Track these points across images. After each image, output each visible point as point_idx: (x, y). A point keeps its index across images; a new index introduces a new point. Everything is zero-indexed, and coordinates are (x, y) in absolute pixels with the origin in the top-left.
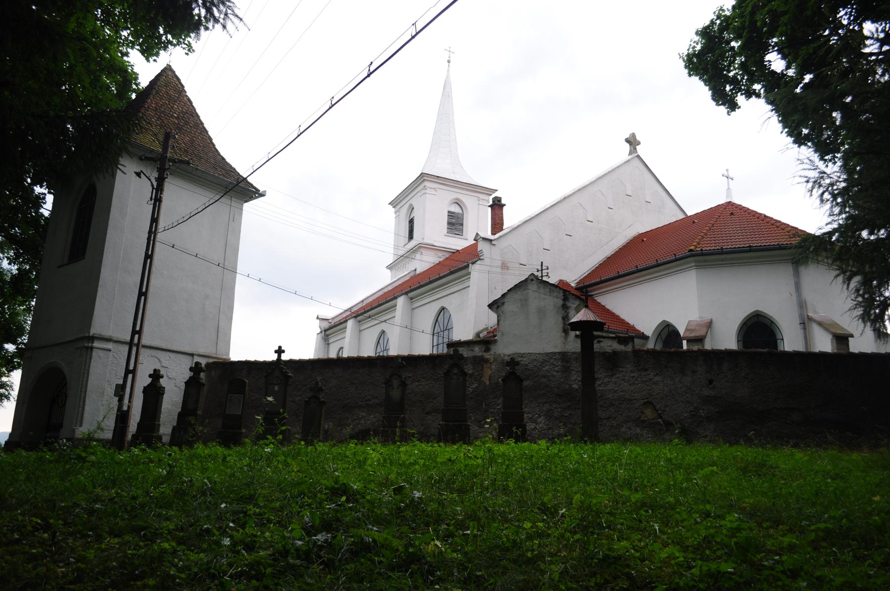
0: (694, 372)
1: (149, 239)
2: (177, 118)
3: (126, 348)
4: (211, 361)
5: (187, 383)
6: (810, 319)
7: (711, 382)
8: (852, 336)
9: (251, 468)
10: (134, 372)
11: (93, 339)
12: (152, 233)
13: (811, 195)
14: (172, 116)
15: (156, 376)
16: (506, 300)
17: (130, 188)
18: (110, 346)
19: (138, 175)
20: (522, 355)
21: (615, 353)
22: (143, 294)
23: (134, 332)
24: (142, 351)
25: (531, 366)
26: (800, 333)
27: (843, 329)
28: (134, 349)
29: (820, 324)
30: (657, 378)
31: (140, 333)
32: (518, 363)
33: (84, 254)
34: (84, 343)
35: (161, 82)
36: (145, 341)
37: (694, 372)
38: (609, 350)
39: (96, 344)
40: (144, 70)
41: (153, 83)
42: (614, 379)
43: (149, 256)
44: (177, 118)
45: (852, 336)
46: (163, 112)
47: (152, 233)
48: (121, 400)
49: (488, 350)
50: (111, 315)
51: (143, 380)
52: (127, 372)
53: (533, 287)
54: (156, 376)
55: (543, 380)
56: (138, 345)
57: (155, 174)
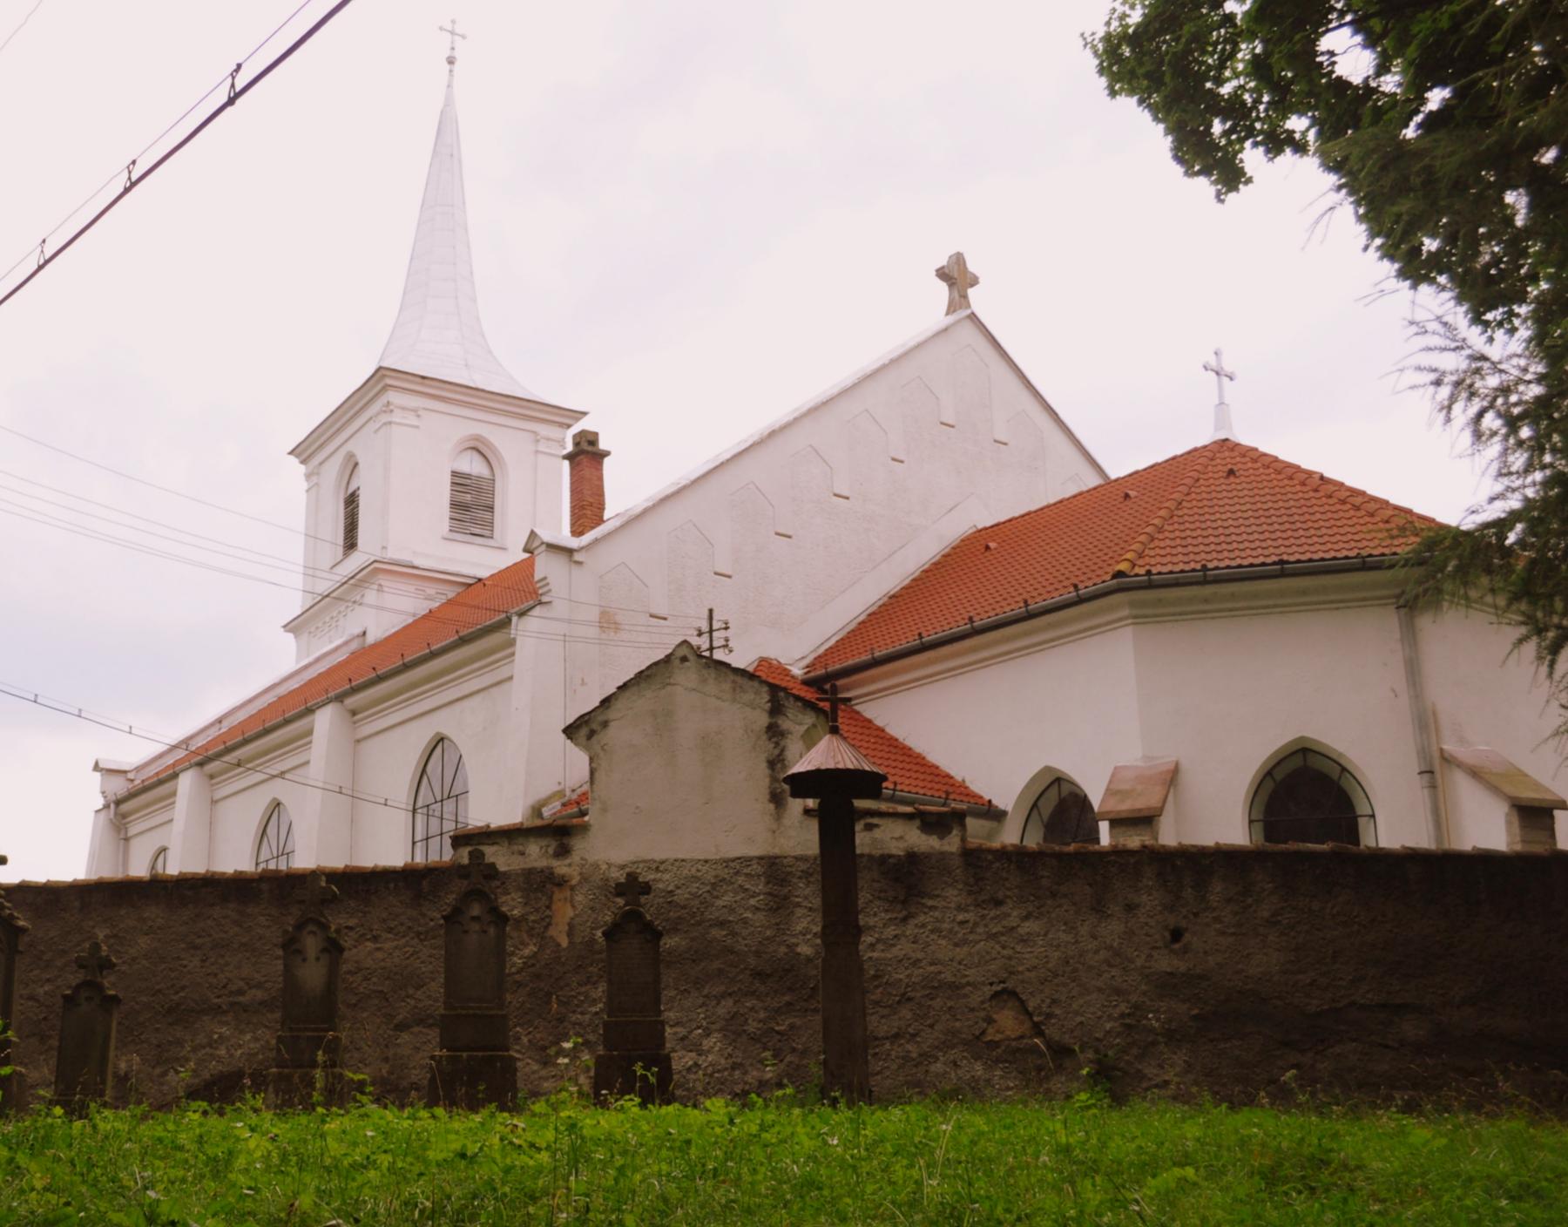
0: (1130, 908)
6: (1448, 760)
7: (1176, 935)
16: (612, 714)
20: (658, 866)
21: (912, 857)
25: (681, 896)
27: (1548, 790)
29: (1475, 773)
32: (646, 888)
37: (1130, 908)
38: (897, 849)
42: (910, 929)
49: (563, 852)
53: (686, 677)
55: (717, 933)
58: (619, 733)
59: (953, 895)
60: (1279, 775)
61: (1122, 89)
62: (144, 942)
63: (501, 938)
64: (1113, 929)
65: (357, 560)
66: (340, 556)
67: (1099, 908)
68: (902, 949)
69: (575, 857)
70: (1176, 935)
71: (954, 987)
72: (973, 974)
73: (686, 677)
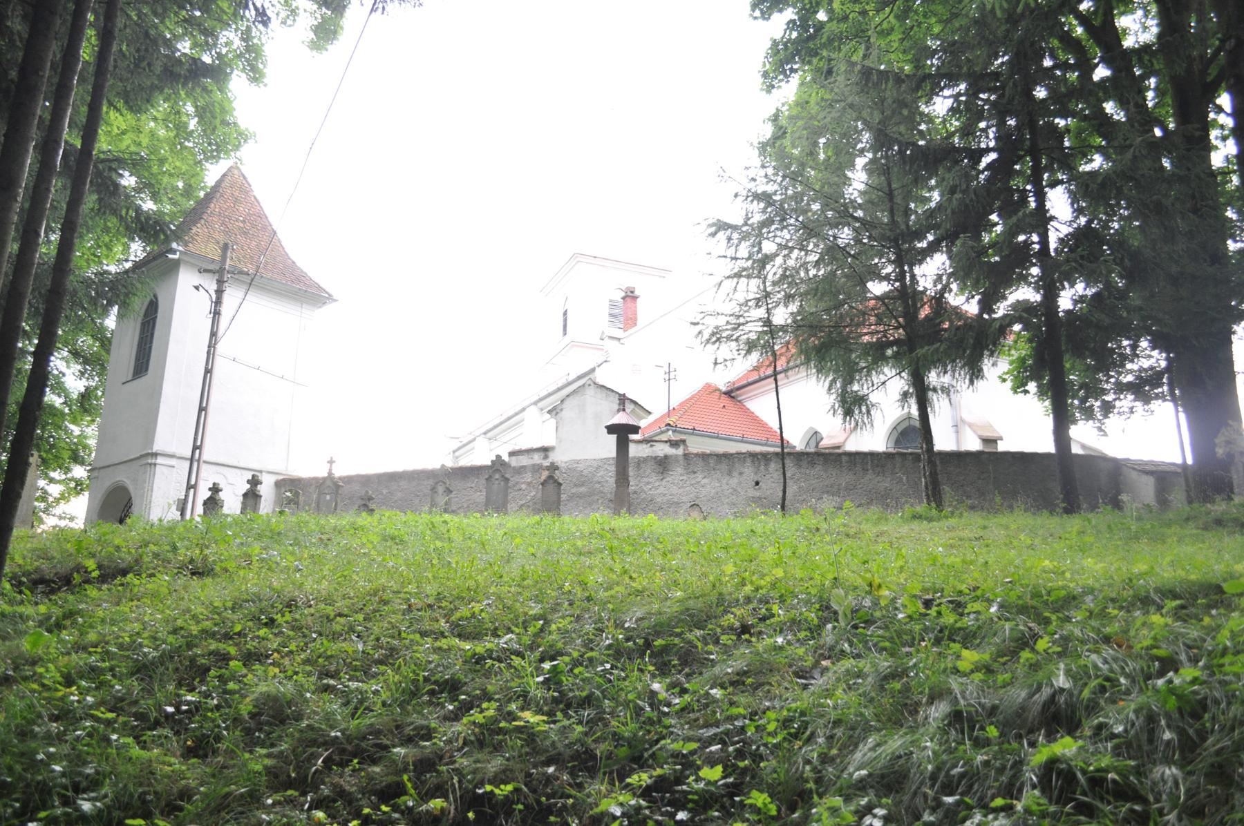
0: (741, 474)
1: (208, 353)
2: (243, 222)
3: (187, 464)
4: (281, 477)
5: (245, 495)
6: (962, 420)
7: (757, 483)
8: (1001, 439)
9: (977, 620)
10: (194, 487)
11: (155, 455)
12: (212, 346)
13: (713, 235)
14: (237, 220)
15: (215, 489)
16: (564, 406)
17: (188, 298)
18: (173, 462)
19: (197, 288)
20: (578, 462)
21: (666, 457)
22: (202, 409)
23: (195, 448)
24: (204, 467)
25: (585, 472)
26: (953, 436)
27: (995, 430)
28: (195, 465)
29: (970, 426)
30: (706, 481)
31: (200, 448)
32: (557, 468)
33: (147, 369)
34: (147, 459)
35: (225, 184)
36: (205, 457)
37: (741, 474)
38: (661, 454)
39: (160, 460)
40: (212, 173)
41: (218, 184)
42: (664, 483)
43: (208, 371)
44: (243, 222)
45: (1001, 439)
46: (227, 217)
47: (212, 346)
48: (182, 514)
49: (546, 457)
50: (171, 434)
51: (204, 494)
52: (189, 487)
53: (591, 391)
54: (215, 489)
55: (597, 486)
56: (199, 461)
57: (215, 287)
58: (568, 412)
59: (679, 470)
60: (900, 429)
61: (959, 103)
62: (399, 494)
63: (507, 488)
64: (734, 481)
65: (568, 338)
66: (130, 377)
67: (730, 474)
68: (661, 490)
69: (550, 460)
70: (757, 483)
71: (678, 503)
72: (684, 499)
73: (591, 391)
